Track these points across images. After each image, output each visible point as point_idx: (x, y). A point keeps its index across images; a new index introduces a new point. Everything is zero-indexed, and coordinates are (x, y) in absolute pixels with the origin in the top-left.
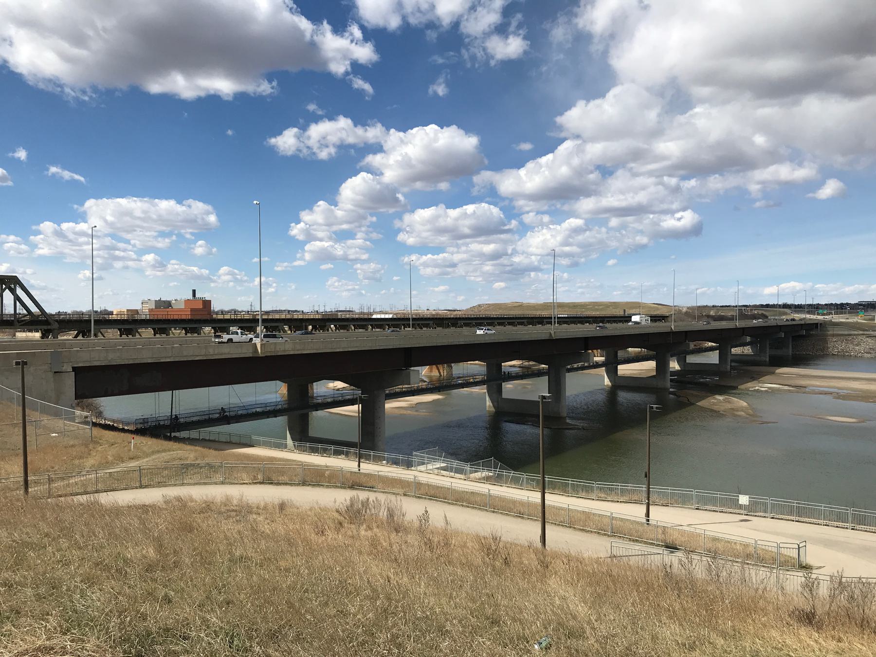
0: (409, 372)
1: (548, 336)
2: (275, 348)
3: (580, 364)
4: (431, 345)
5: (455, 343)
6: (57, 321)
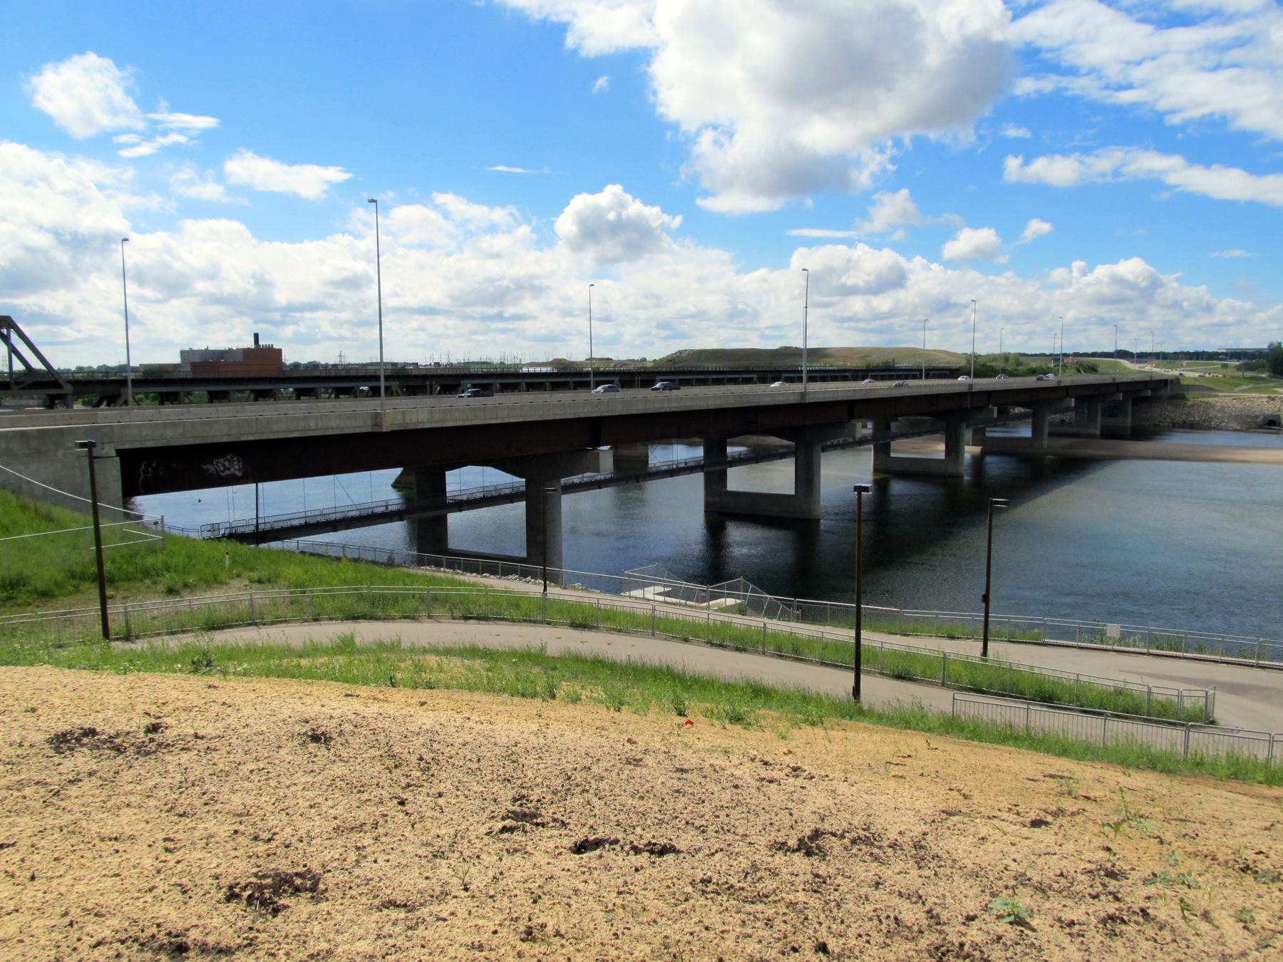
0: (598, 454)
1: (369, 423)
2: (404, 418)
3: (841, 440)
4: (610, 414)
5: (664, 410)
6: (70, 382)
